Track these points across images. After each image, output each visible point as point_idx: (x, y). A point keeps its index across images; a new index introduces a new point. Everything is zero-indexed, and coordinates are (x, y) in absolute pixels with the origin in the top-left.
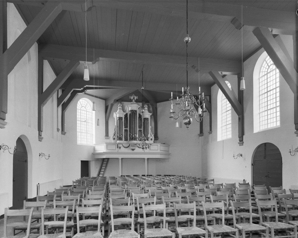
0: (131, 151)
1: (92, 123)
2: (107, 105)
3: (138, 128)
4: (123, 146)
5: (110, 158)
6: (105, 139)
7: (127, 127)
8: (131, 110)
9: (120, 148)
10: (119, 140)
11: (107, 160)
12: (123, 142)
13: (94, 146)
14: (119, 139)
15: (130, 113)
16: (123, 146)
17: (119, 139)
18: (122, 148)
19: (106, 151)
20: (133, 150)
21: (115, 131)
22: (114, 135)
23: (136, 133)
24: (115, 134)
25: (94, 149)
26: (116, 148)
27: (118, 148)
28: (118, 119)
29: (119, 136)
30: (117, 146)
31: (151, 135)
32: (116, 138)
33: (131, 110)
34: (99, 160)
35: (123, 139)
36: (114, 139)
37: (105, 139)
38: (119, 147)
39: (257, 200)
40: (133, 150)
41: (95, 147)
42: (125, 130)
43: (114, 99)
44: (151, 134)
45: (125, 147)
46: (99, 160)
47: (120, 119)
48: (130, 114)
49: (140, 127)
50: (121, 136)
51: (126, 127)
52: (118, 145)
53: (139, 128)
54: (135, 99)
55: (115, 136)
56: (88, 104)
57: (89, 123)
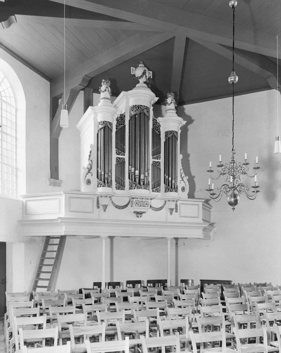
0: (134, 217)
1: (16, 138)
2: (58, 93)
3: (151, 157)
4: (113, 203)
5: (68, 235)
6: (50, 185)
7: (124, 151)
8: (134, 107)
9: (105, 207)
10: (103, 184)
11: (57, 241)
12: (113, 190)
13: (24, 200)
14: (104, 182)
15: (133, 113)
16: (113, 203)
17: (104, 182)
18: (111, 208)
19: (66, 217)
20: (139, 214)
21: (91, 160)
22: (89, 172)
23: (148, 170)
24: (91, 168)
25: (25, 209)
26: (93, 208)
27: (98, 207)
28: (100, 126)
29: (103, 173)
30: (98, 201)
31: (182, 178)
32: (94, 180)
33: (138, 104)
34: (35, 241)
35: (114, 183)
36: (89, 182)
37: (50, 185)
38: (101, 207)
39: (227, 304)
40: (139, 214)
41: (26, 205)
42: (118, 160)
43: (83, 76)
44: (183, 175)
45: (118, 207)
46: (35, 241)
47: (106, 127)
48: (133, 118)
49: (156, 153)
50: (108, 174)
51: (120, 149)
52: (100, 199)
53: (153, 158)
54: (146, 77)
55: (90, 174)
56: (5, 80)
57: (7, 134)
